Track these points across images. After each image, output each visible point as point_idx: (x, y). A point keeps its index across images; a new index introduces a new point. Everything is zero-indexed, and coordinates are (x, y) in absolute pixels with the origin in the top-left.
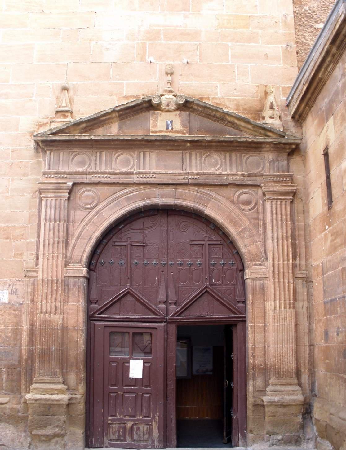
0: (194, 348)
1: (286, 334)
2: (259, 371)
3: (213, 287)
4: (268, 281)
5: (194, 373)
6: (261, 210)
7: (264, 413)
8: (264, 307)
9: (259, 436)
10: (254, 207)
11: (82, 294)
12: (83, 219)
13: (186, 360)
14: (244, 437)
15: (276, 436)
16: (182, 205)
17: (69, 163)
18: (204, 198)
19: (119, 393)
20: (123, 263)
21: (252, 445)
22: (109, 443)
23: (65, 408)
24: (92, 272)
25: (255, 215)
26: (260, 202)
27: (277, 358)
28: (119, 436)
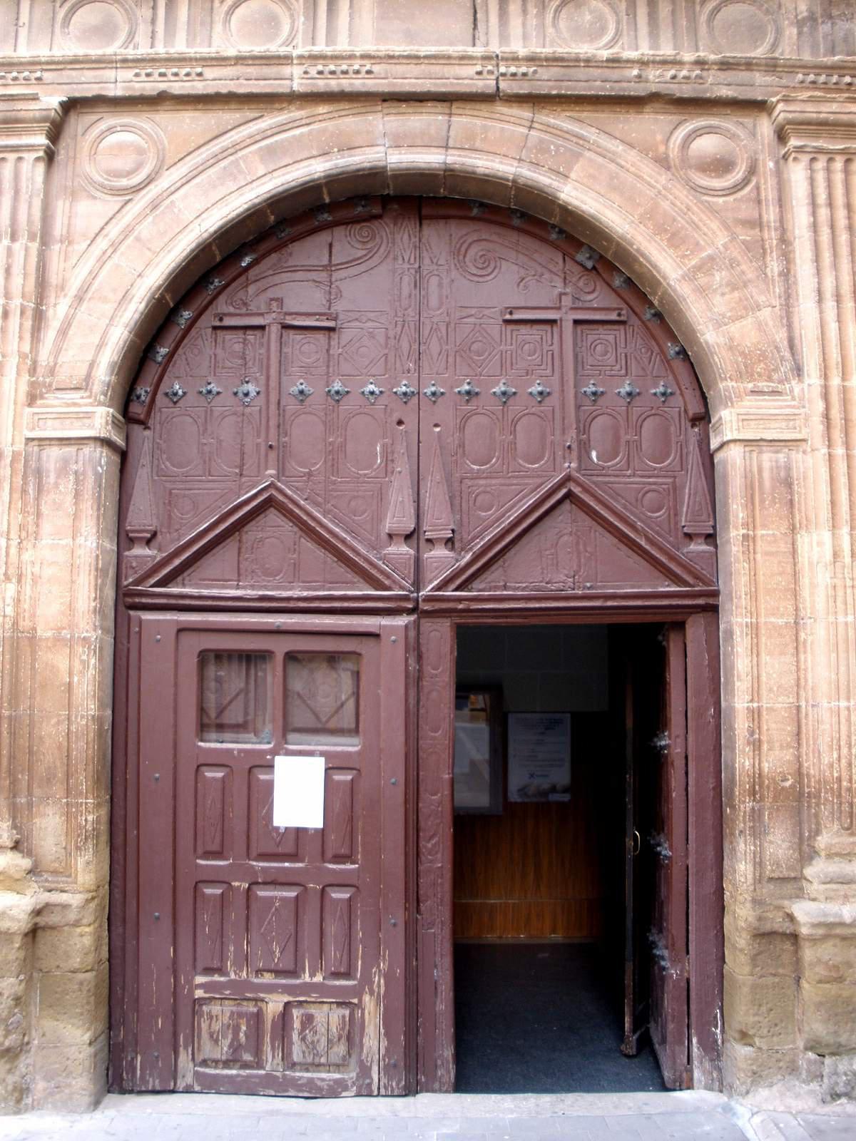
0: (512, 720)
2: (775, 799)
3: (595, 479)
4: (804, 452)
5: (514, 797)
6: (769, 193)
7: (797, 963)
8: (794, 552)
9: (779, 1056)
10: (745, 182)
11: (89, 503)
12: (102, 229)
13: (487, 756)
14: (713, 1051)
15: (846, 1058)
16: (474, 173)
17: (53, 33)
18: (557, 147)
19: (236, 884)
20: (253, 394)
21: (747, 1093)
22: (196, 1073)
23: (17, 945)
24: (137, 429)
25: (747, 211)
26: (765, 166)
28: (236, 1047)
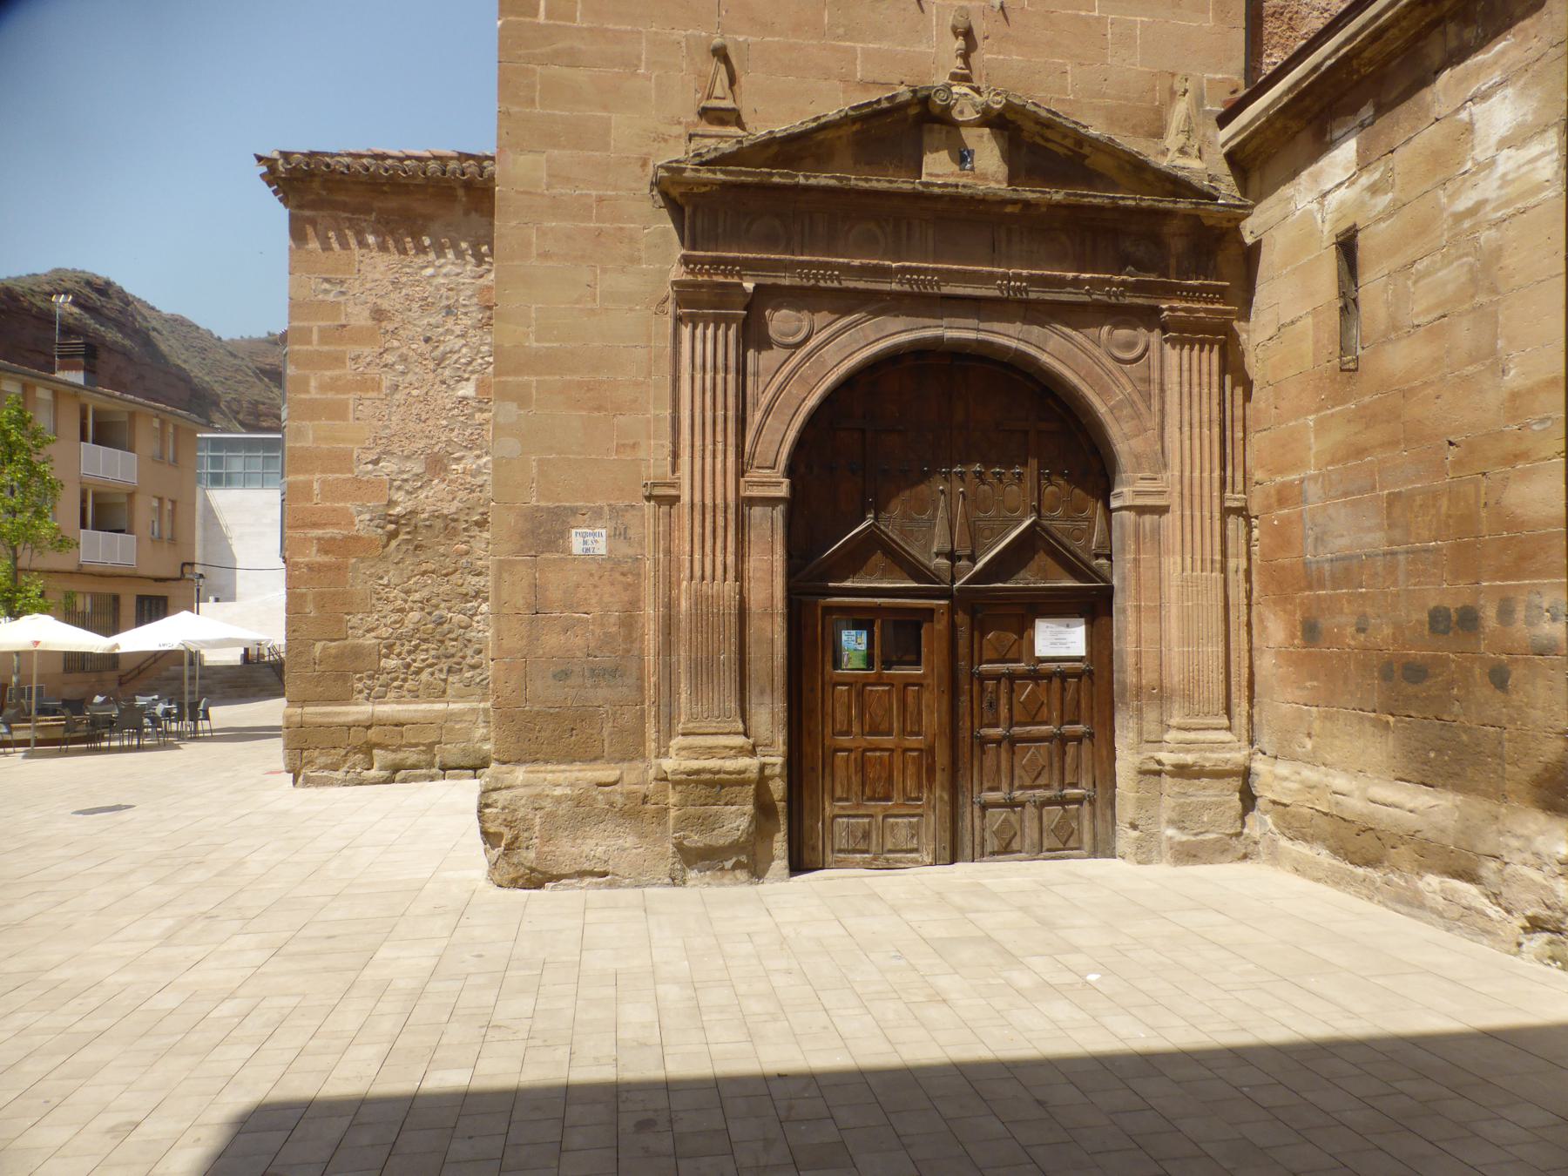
1: (1205, 625)
6: (1155, 363)
27: (1186, 675)
